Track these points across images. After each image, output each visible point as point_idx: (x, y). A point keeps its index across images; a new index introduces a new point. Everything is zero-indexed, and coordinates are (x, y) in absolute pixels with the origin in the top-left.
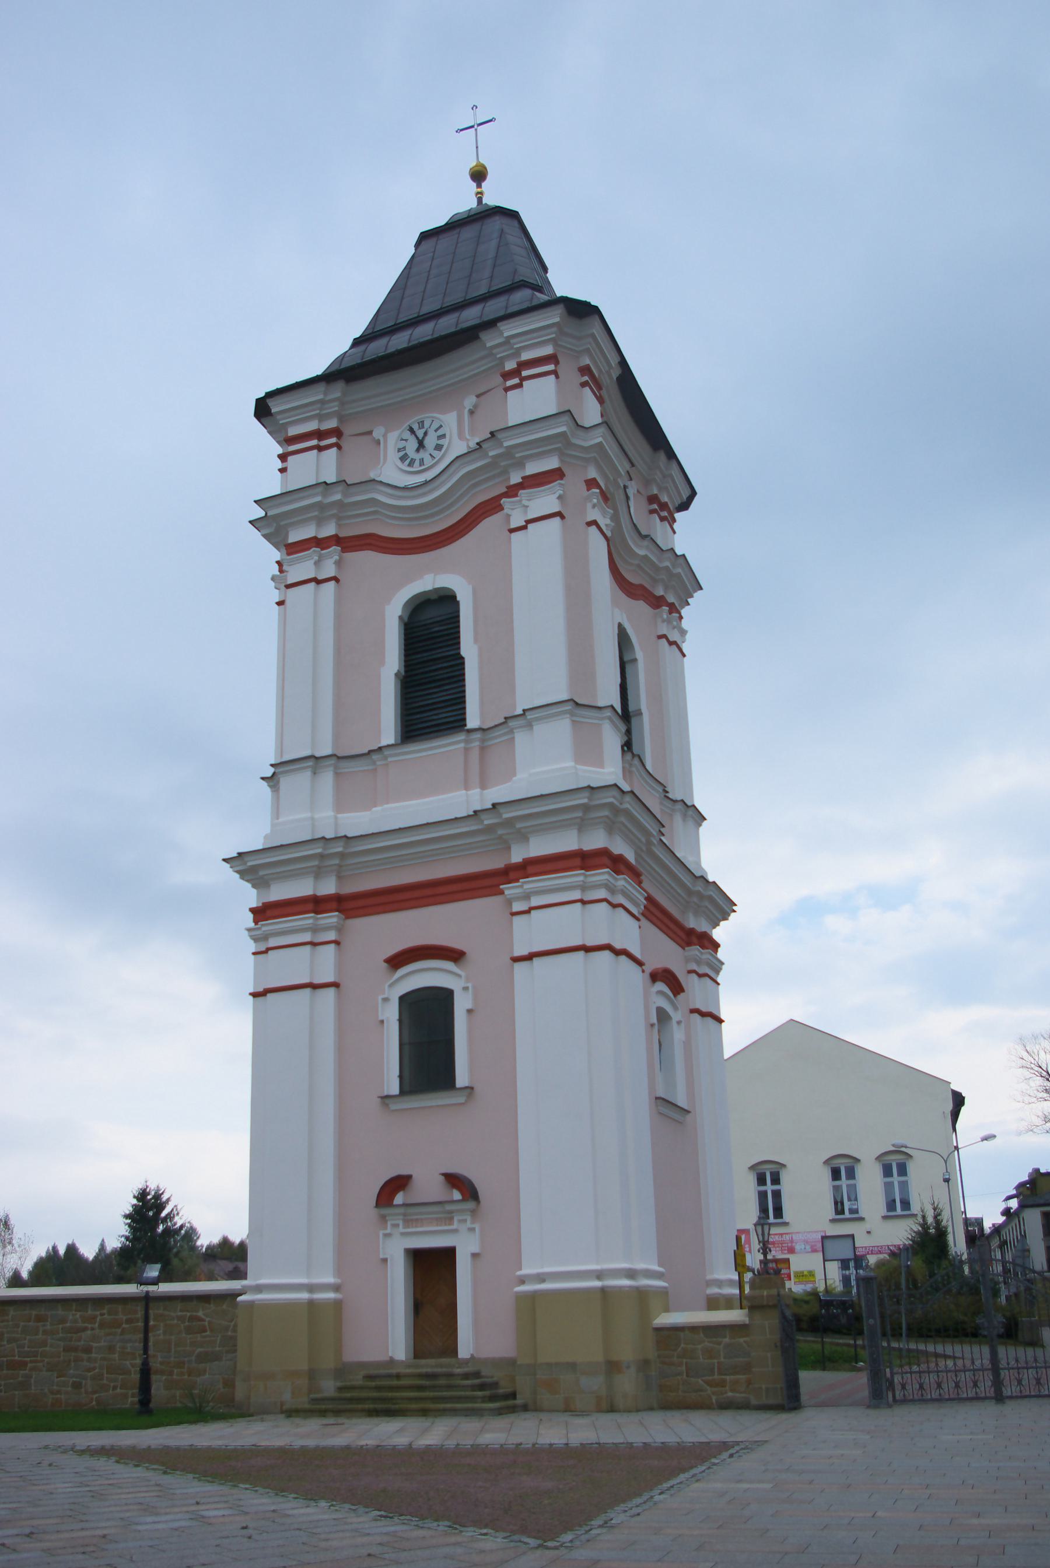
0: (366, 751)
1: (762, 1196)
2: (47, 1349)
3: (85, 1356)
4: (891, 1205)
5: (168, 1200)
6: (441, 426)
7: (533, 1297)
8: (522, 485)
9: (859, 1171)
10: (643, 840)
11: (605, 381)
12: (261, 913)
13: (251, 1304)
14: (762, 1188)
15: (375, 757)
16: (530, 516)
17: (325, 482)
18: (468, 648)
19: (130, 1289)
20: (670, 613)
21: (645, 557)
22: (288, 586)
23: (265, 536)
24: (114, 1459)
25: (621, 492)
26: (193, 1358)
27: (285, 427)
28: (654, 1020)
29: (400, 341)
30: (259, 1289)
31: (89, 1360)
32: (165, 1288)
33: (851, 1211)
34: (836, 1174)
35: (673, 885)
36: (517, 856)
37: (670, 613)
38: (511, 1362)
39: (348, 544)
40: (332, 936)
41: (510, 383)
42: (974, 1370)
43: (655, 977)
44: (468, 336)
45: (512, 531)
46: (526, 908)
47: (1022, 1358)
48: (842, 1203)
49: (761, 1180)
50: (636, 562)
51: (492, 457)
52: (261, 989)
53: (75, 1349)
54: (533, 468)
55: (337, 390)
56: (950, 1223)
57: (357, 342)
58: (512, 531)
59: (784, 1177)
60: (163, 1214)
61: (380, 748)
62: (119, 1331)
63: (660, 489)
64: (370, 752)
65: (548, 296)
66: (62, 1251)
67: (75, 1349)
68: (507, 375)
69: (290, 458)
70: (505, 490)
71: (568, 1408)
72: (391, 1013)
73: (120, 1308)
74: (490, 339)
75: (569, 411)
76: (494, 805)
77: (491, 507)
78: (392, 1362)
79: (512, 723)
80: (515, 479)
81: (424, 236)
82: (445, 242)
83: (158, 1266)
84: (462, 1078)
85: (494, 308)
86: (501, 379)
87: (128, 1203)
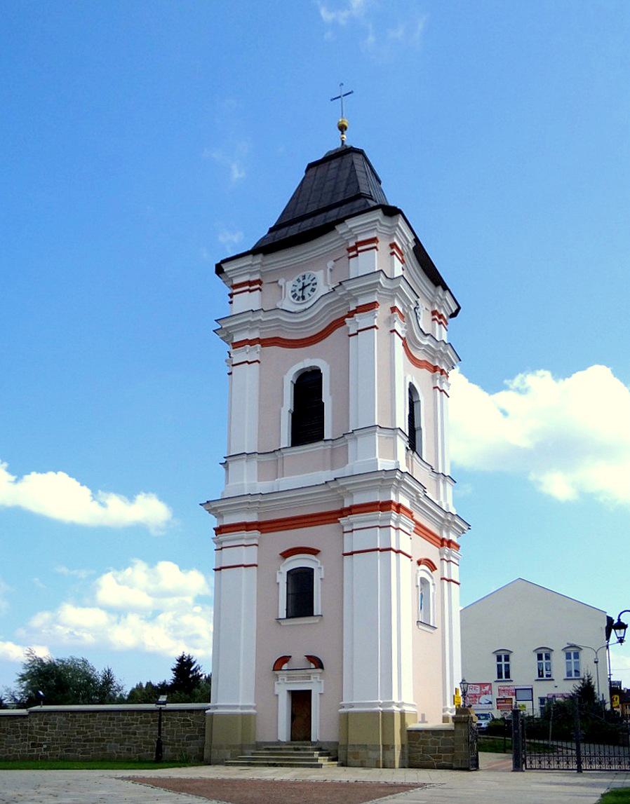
0: (272, 450)
1: (499, 667)
2: (115, 733)
3: (133, 736)
4: (569, 674)
5: (194, 662)
6: (314, 278)
7: (347, 715)
8: (355, 312)
9: (553, 656)
10: (414, 496)
11: (406, 250)
12: (219, 530)
13: (212, 715)
14: (499, 663)
15: (277, 453)
16: (359, 328)
17: (252, 310)
18: (326, 398)
19: (152, 706)
20: (442, 374)
21: (428, 345)
22: (233, 365)
23: (222, 338)
24: (131, 781)
25: (413, 312)
26: (185, 739)
27: (231, 279)
28: (419, 584)
29: (293, 231)
30: (216, 707)
31: (135, 738)
32: (170, 706)
33: (547, 676)
34: (540, 657)
35: (433, 516)
36: (347, 505)
37: (442, 374)
38: (337, 743)
39: (265, 343)
40: (255, 542)
41: (351, 254)
42: (568, 756)
43: (419, 563)
44: (329, 228)
45: (350, 336)
46: (351, 530)
47: (612, 752)
48: (542, 671)
49: (499, 659)
50: (423, 348)
51: (341, 295)
52: (218, 567)
53: (128, 733)
54: (362, 302)
55: (259, 258)
56: (596, 684)
57: (271, 230)
58: (350, 336)
59: (511, 658)
60: (192, 669)
61: (280, 449)
62: (149, 725)
63: (439, 307)
64: (274, 451)
65: (376, 202)
66: (144, 686)
67: (128, 733)
68: (350, 250)
69: (234, 296)
70: (347, 313)
71: (362, 766)
72: (282, 580)
73: (150, 714)
74: (340, 229)
75: (382, 270)
76: (335, 479)
77: (340, 323)
78: (279, 743)
79: (346, 437)
80: (353, 308)
81: (311, 166)
82: (320, 171)
83: (166, 696)
84: (317, 608)
85: (344, 210)
86: (347, 252)
87: (174, 664)
